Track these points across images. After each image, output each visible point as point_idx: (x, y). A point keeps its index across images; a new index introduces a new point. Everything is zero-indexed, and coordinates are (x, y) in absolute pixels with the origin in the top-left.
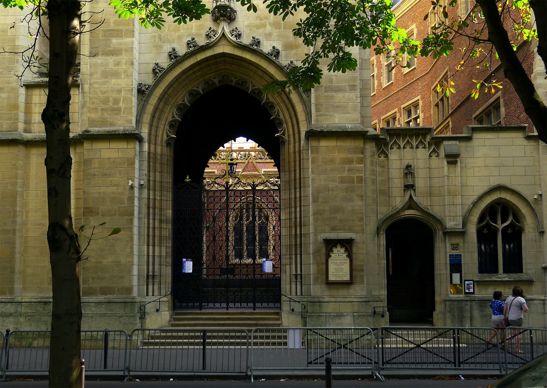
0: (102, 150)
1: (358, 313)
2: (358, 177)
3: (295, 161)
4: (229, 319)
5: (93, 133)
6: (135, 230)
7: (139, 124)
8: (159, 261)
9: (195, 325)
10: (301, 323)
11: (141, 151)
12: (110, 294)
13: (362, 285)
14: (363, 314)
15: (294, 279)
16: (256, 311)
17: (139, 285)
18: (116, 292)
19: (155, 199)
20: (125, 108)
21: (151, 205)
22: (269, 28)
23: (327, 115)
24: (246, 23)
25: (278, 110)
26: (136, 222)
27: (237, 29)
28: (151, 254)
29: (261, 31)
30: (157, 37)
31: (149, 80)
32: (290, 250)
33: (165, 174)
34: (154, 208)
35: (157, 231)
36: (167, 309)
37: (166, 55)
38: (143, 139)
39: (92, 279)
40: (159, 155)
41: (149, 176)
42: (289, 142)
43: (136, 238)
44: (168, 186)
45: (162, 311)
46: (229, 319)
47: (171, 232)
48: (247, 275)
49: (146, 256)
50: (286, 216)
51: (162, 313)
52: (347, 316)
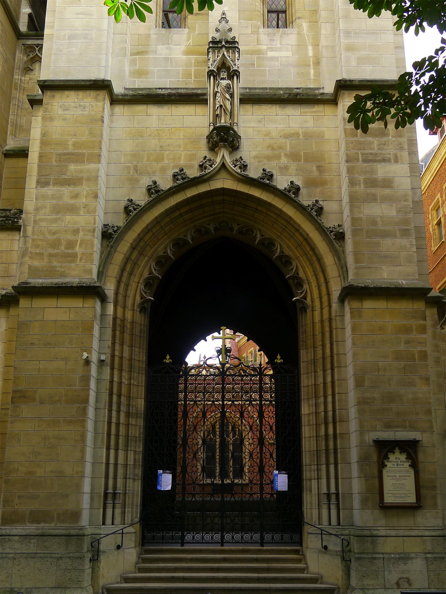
0: (46, 309)
1: (432, 553)
2: (420, 352)
3: (323, 333)
4: (225, 560)
5: (34, 285)
6: (90, 426)
7: (102, 276)
8: (123, 473)
9: (175, 570)
10: (340, 569)
11: (103, 315)
12: (46, 522)
13: (434, 511)
14: (440, 555)
15: (324, 500)
16: (265, 548)
17: (91, 508)
18: (55, 519)
19: (120, 383)
20: (83, 254)
21: (115, 390)
22: (284, 160)
23: (371, 267)
24: (253, 154)
25: (297, 266)
26: (91, 413)
27: (242, 160)
28: (112, 461)
29: (274, 163)
30: (132, 169)
31: (120, 221)
32: (317, 457)
33: (137, 349)
34: (119, 396)
35: (122, 429)
36: (133, 545)
37: (144, 190)
38: (107, 298)
39: (19, 498)
40: (129, 324)
41: (113, 350)
42: (313, 307)
43: (90, 436)
44: (141, 365)
45: (125, 549)
46: (225, 560)
47: (142, 430)
48: (251, 495)
49: (104, 464)
50: (309, 410)
51: (126, 551)
52: (417, 558)
